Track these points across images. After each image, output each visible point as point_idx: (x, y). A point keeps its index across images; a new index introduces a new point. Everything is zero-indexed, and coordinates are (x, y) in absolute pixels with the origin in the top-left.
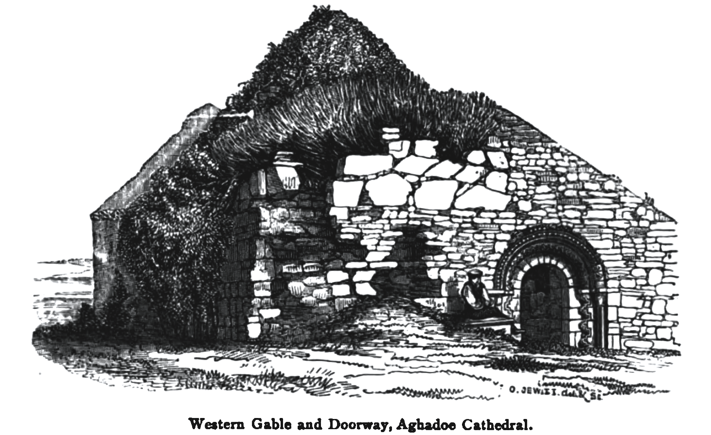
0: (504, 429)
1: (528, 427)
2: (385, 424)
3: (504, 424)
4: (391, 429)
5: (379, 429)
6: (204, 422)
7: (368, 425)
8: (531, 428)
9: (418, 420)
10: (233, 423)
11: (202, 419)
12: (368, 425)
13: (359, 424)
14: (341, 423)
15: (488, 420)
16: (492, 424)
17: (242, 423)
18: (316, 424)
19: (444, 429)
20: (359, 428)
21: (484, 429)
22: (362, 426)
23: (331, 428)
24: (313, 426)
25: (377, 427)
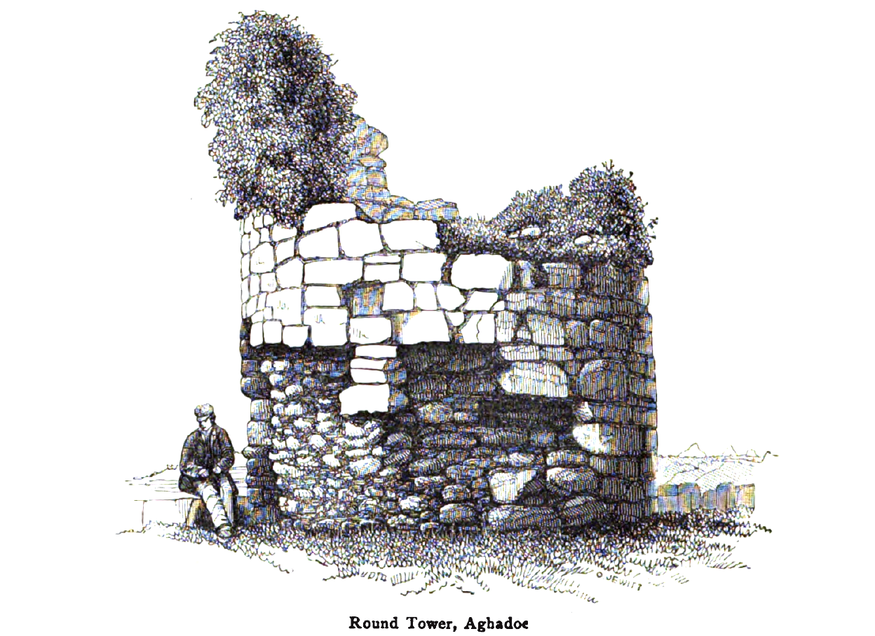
1: (409, 619)
4: (455, 628)
9: (488, 618)
18: (506, 623)
19: (517, 628)
24: (427, 624)
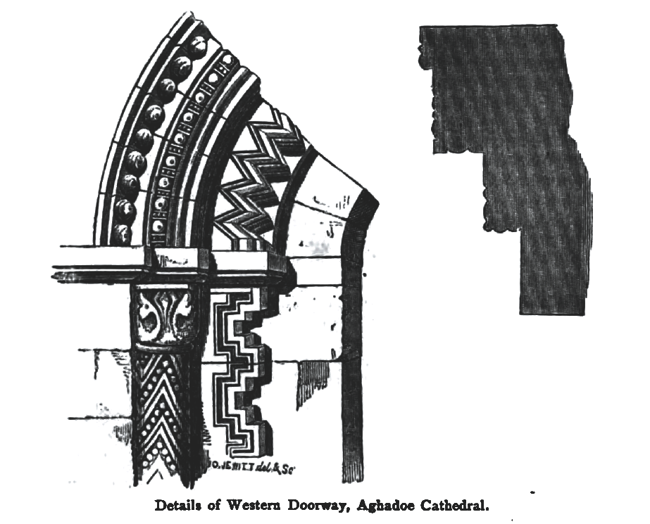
0: (462, 510)
1: (485, 508)
2: (343, 505)
3: (461, 504)
4: (348, 510)
5: (338, 509)
6: (242, 504)
7: (326, 506)
8: (487, 509)
10: (270, 504)
11: (240, 501)
12: (326, 506)
13: (317, 504)
14: (167, 504)
15: (446, 501)
16: (450, 505)
17: (278, 504)
20: (317, 509)
21: (442, 509)
22: (320, 507)
23: (291, 508)
25: (335, 507)
